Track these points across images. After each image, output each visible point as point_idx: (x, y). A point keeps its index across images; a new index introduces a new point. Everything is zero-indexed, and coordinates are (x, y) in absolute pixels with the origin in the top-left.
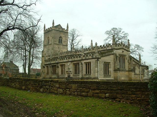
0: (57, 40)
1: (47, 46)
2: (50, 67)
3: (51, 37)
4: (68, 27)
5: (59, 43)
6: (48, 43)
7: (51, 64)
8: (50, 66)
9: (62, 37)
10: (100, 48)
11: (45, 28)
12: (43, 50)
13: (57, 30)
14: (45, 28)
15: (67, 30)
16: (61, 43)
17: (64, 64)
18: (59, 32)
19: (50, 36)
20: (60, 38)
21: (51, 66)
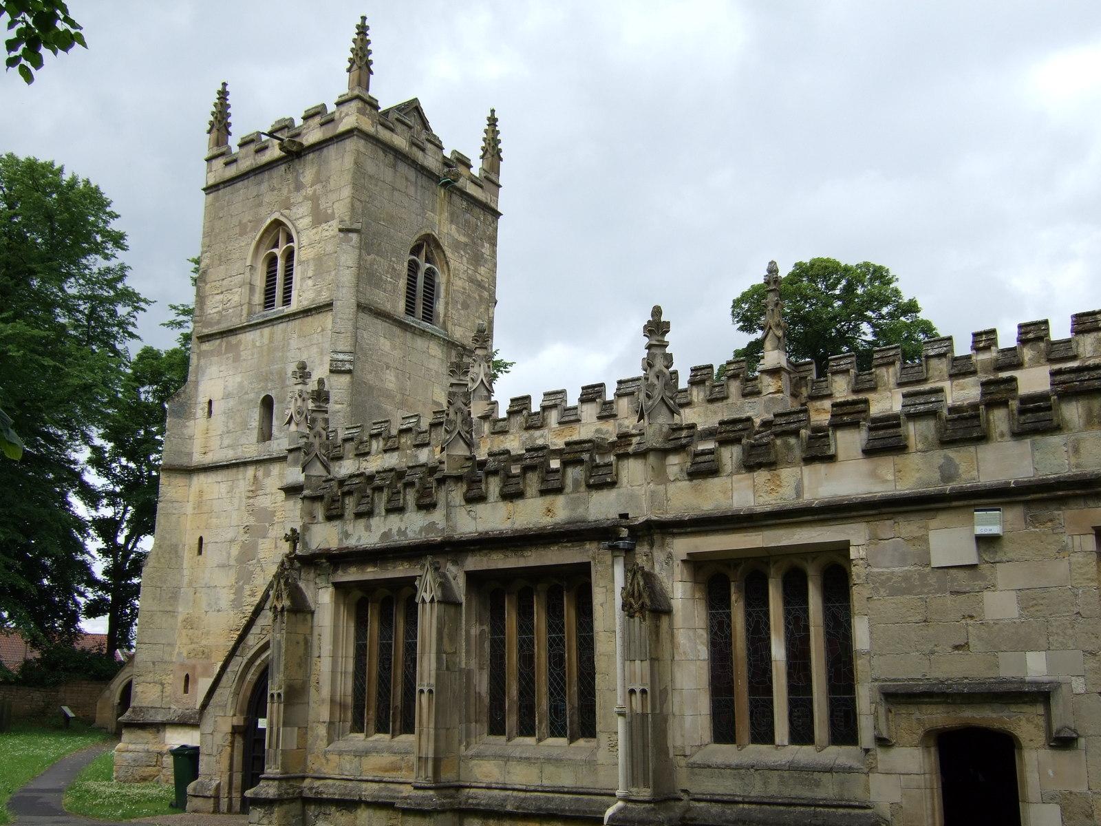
0: (399, 276)
1: (248, 337)
2: (448, 601)
3: (319, 218)
4: (492, 150)
5: (410, 310)
6: (259, 298)
7: (455, 548)
8: (445, 586)
9: (445, 243)
10: (698, 395)
11: (221, 123)
12: (190, 788)
13: (398, 154)
14: (221, 123)
15: (491, 180)
16: (429, 315)
17: (399, 571)
18: (412, 174)
19: (300, 219)
20: (416, 250)
21: (459, 586)
